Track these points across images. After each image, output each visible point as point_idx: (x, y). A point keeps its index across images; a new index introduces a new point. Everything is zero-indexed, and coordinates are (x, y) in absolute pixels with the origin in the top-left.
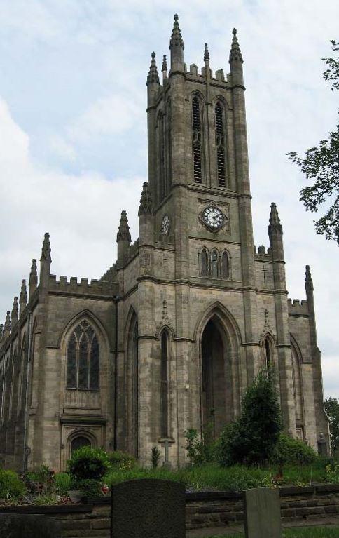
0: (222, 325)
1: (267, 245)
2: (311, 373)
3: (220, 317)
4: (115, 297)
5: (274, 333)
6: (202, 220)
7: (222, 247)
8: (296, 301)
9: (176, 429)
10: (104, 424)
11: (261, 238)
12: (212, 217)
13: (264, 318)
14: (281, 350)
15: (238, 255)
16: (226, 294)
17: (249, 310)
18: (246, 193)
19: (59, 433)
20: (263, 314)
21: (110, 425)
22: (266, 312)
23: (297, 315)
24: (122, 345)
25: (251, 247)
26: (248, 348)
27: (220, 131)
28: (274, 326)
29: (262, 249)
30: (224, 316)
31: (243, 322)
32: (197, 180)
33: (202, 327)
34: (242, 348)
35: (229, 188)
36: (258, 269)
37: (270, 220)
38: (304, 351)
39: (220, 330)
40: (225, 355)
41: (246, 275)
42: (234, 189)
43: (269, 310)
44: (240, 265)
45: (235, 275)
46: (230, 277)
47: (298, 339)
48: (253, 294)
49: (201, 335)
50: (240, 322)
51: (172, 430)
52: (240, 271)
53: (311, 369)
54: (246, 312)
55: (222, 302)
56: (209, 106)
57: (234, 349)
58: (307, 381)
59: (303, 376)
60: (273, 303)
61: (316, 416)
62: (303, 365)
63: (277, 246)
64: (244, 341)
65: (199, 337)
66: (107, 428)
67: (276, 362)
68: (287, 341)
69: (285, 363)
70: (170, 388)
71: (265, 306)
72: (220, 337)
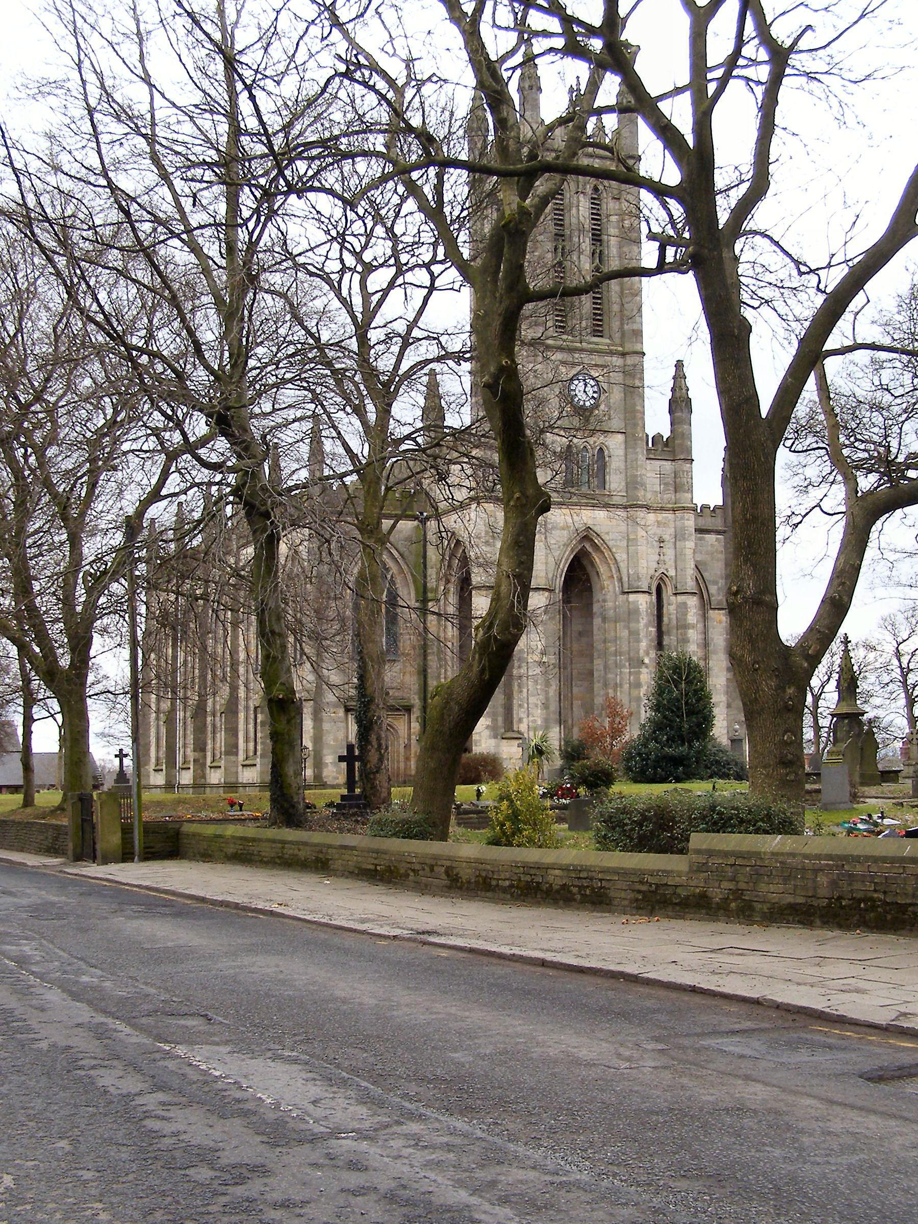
0: (593, 564)
1: (666, 434)
2: (724, 624)
3: (590, 550)
4: (422, 514)
5: (672, 573)
6: (568, 397)
7: (597, 440)
8: (705, 507)
9: (525, 720)
10: (408, 709)
11: (657, 421)
12: (583, 393)
13: (658, 550)
14: (680, 598)
15: (621, 452)
16: (601, 514)
17: (636, 540)
18: (637, 348)
19: (344, 724)
20: (656, 544)
21: (416, 713)
22: (661, 541)
23: (708, 531)
24: (436, 590)
25: (641, 439)
26: (632, 597)
27: (597, 238)
28: (672, 563)
29: (657, 438)
30: (596, 547)
31: (625, 556)
32: (560, 327)
33: (564, 566)
34: (622, 598)
35: (610, 338)
36: (652, 473)
37: (673, 390)
38: (713, 589)
39: (589, 568)
40: (596, 608)
41: (633, 484)
42: (618, 341)
43: (666, 537)
44: (623, 467)
45: (615, 482)
46: (607, 487)
47: (706, 570)
48: (641, 513)
49: (827, 1010)
50: (621, 556)
51: (520, 720)
52: (623, 475)
53: (724, 619)
54: (630, 541)
55: (595, 529)
56: (581, 197)
57: (607, 592)
58: (716, 637)
59: (711, 630)
60: (672, 525)
61: (727, 693)
62: (711, 612)
63: (683, 434)
64: (626, 585)
65: (559, 582)
66: (413, 717)
67: (674, 617)
68: (691, 585)
69: (685, 620)
70: (519, 660)
71: (659, 531)
72: (588, 580)
